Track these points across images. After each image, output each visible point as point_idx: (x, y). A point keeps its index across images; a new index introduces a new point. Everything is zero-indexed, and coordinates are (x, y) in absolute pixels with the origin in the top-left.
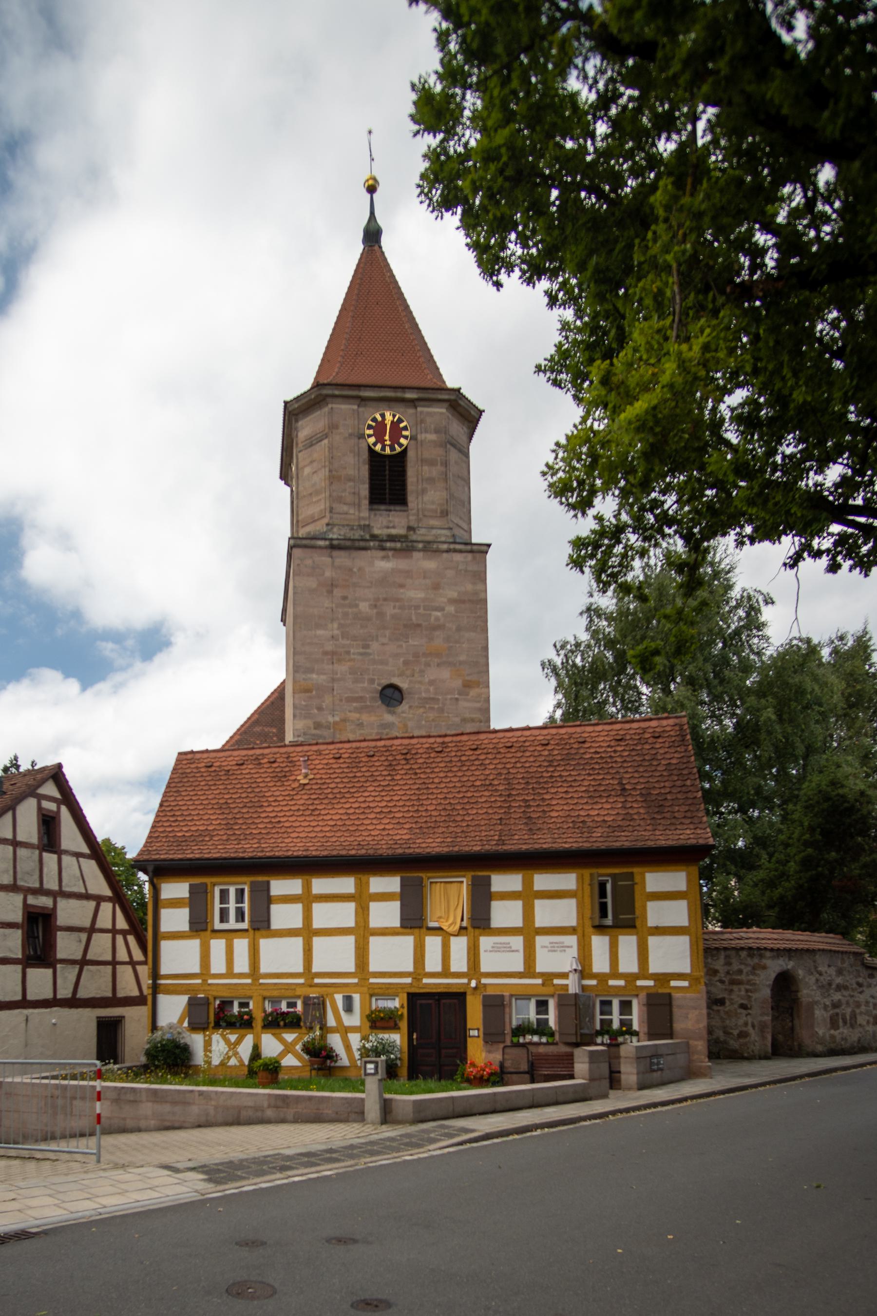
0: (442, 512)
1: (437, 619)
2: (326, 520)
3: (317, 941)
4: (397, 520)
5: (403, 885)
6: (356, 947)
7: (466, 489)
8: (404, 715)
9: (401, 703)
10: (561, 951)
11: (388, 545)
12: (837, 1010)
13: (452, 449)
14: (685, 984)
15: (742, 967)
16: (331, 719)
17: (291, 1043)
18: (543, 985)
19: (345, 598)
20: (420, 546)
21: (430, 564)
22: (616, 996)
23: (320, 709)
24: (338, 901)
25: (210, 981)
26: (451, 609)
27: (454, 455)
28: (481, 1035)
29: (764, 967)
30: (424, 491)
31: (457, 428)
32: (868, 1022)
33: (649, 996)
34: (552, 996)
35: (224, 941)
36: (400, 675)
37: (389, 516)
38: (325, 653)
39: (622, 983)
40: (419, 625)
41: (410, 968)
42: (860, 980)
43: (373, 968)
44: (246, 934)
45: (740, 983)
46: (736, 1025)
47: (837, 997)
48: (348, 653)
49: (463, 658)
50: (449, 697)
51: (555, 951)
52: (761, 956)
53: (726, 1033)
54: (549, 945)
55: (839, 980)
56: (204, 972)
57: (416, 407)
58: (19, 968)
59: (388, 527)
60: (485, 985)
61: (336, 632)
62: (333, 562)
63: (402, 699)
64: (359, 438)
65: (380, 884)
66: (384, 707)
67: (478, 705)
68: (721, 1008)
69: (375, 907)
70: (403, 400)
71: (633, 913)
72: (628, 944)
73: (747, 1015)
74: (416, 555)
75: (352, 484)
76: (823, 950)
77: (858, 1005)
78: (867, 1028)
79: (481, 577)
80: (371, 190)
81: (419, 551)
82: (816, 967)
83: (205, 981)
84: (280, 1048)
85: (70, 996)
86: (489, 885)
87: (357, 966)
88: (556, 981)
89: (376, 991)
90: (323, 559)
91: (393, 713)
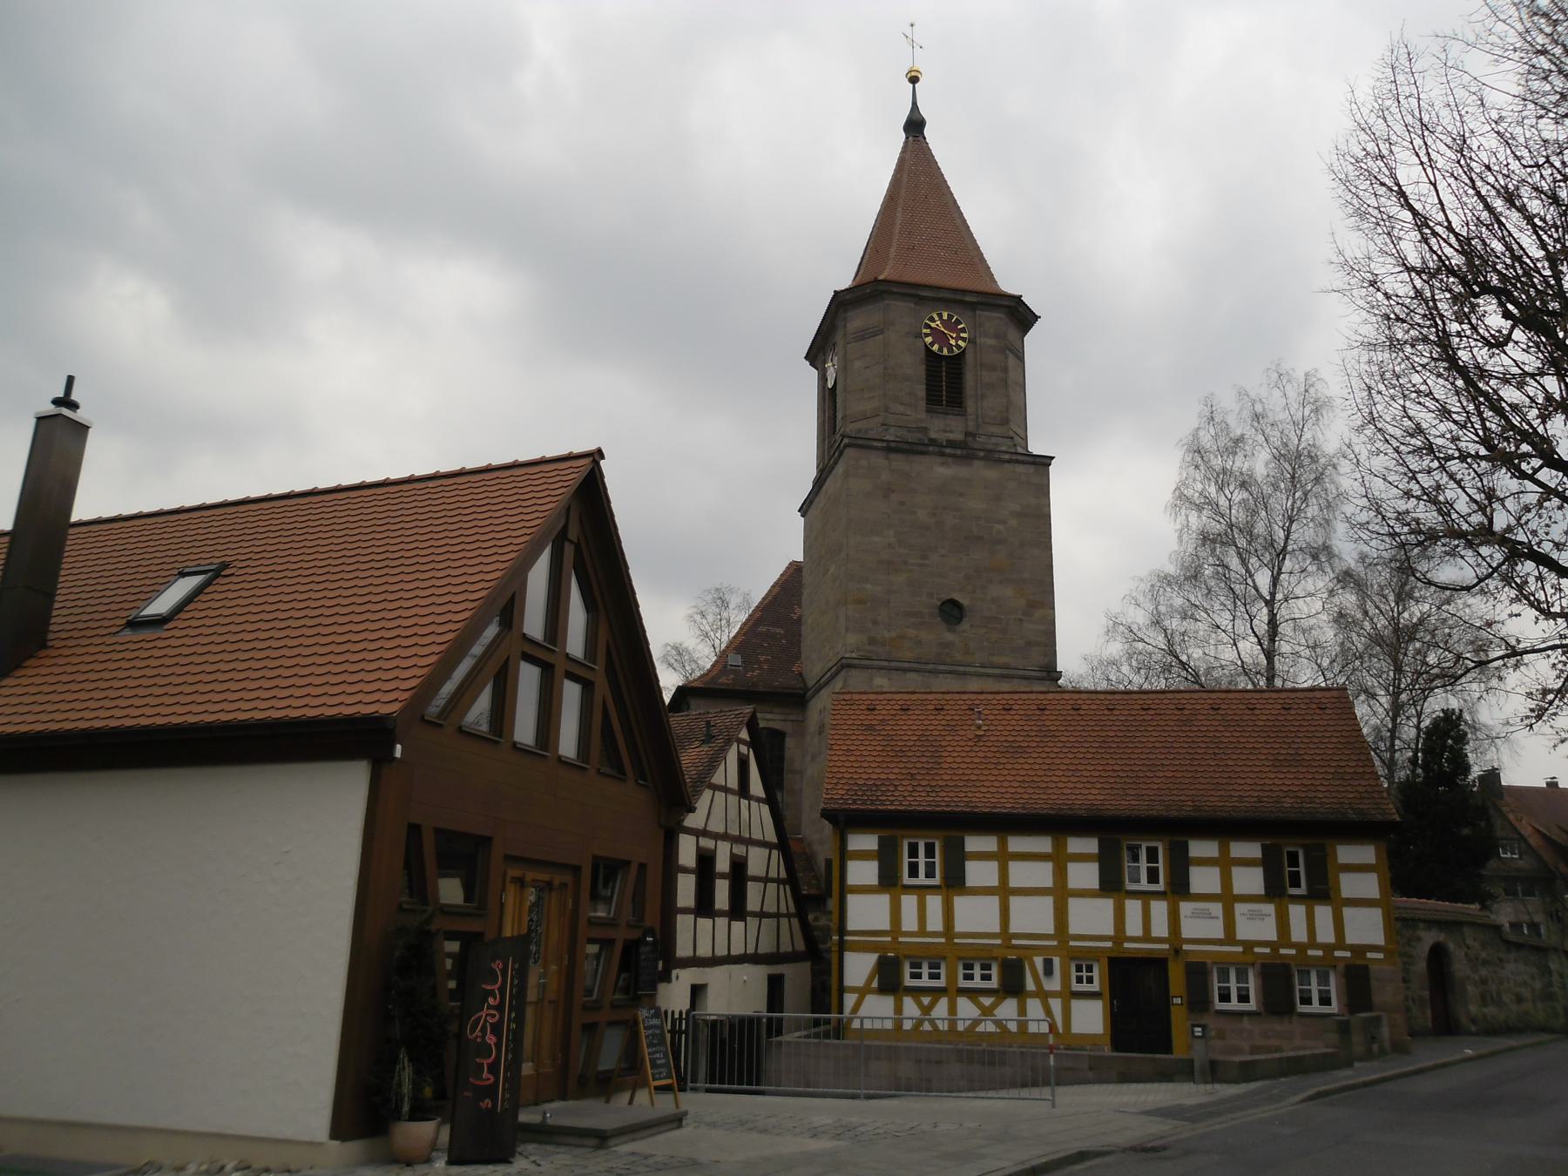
5: (1100, 847)
7: (1022, 394)
8: (965, 634)
10: (1260, 919)
11: (948, 451)
13: (1010, 354)
14: (1381, 956)
16: (887, 635)
19: (902, 503)
20: (982, 454)
21: (992, 474)
23: (875, 623)
25: (901, 939)
26: (1014, 522)
27: (1012, 360)
33: (1263, 965)
39: (1320, 953)
41: (1110, 931)
47: (1484, 972)
51: (1253, 919)
55: (1483, 955)
57: (974, 311)
58: (692, 917)
59: (945, 431)
60: (1187, 952)
64: (916, 337)
65: (1076, 845)
70: (961, 302)
71: (1327, 884)
72: (1323, 913)
74: (977, 463)
79: (1044, 491)
80: (914, 80)
82: (1464, 940)
83: (895, 939)
86: (1187, 851)
88: (1257, 950)
90: (878, 460)
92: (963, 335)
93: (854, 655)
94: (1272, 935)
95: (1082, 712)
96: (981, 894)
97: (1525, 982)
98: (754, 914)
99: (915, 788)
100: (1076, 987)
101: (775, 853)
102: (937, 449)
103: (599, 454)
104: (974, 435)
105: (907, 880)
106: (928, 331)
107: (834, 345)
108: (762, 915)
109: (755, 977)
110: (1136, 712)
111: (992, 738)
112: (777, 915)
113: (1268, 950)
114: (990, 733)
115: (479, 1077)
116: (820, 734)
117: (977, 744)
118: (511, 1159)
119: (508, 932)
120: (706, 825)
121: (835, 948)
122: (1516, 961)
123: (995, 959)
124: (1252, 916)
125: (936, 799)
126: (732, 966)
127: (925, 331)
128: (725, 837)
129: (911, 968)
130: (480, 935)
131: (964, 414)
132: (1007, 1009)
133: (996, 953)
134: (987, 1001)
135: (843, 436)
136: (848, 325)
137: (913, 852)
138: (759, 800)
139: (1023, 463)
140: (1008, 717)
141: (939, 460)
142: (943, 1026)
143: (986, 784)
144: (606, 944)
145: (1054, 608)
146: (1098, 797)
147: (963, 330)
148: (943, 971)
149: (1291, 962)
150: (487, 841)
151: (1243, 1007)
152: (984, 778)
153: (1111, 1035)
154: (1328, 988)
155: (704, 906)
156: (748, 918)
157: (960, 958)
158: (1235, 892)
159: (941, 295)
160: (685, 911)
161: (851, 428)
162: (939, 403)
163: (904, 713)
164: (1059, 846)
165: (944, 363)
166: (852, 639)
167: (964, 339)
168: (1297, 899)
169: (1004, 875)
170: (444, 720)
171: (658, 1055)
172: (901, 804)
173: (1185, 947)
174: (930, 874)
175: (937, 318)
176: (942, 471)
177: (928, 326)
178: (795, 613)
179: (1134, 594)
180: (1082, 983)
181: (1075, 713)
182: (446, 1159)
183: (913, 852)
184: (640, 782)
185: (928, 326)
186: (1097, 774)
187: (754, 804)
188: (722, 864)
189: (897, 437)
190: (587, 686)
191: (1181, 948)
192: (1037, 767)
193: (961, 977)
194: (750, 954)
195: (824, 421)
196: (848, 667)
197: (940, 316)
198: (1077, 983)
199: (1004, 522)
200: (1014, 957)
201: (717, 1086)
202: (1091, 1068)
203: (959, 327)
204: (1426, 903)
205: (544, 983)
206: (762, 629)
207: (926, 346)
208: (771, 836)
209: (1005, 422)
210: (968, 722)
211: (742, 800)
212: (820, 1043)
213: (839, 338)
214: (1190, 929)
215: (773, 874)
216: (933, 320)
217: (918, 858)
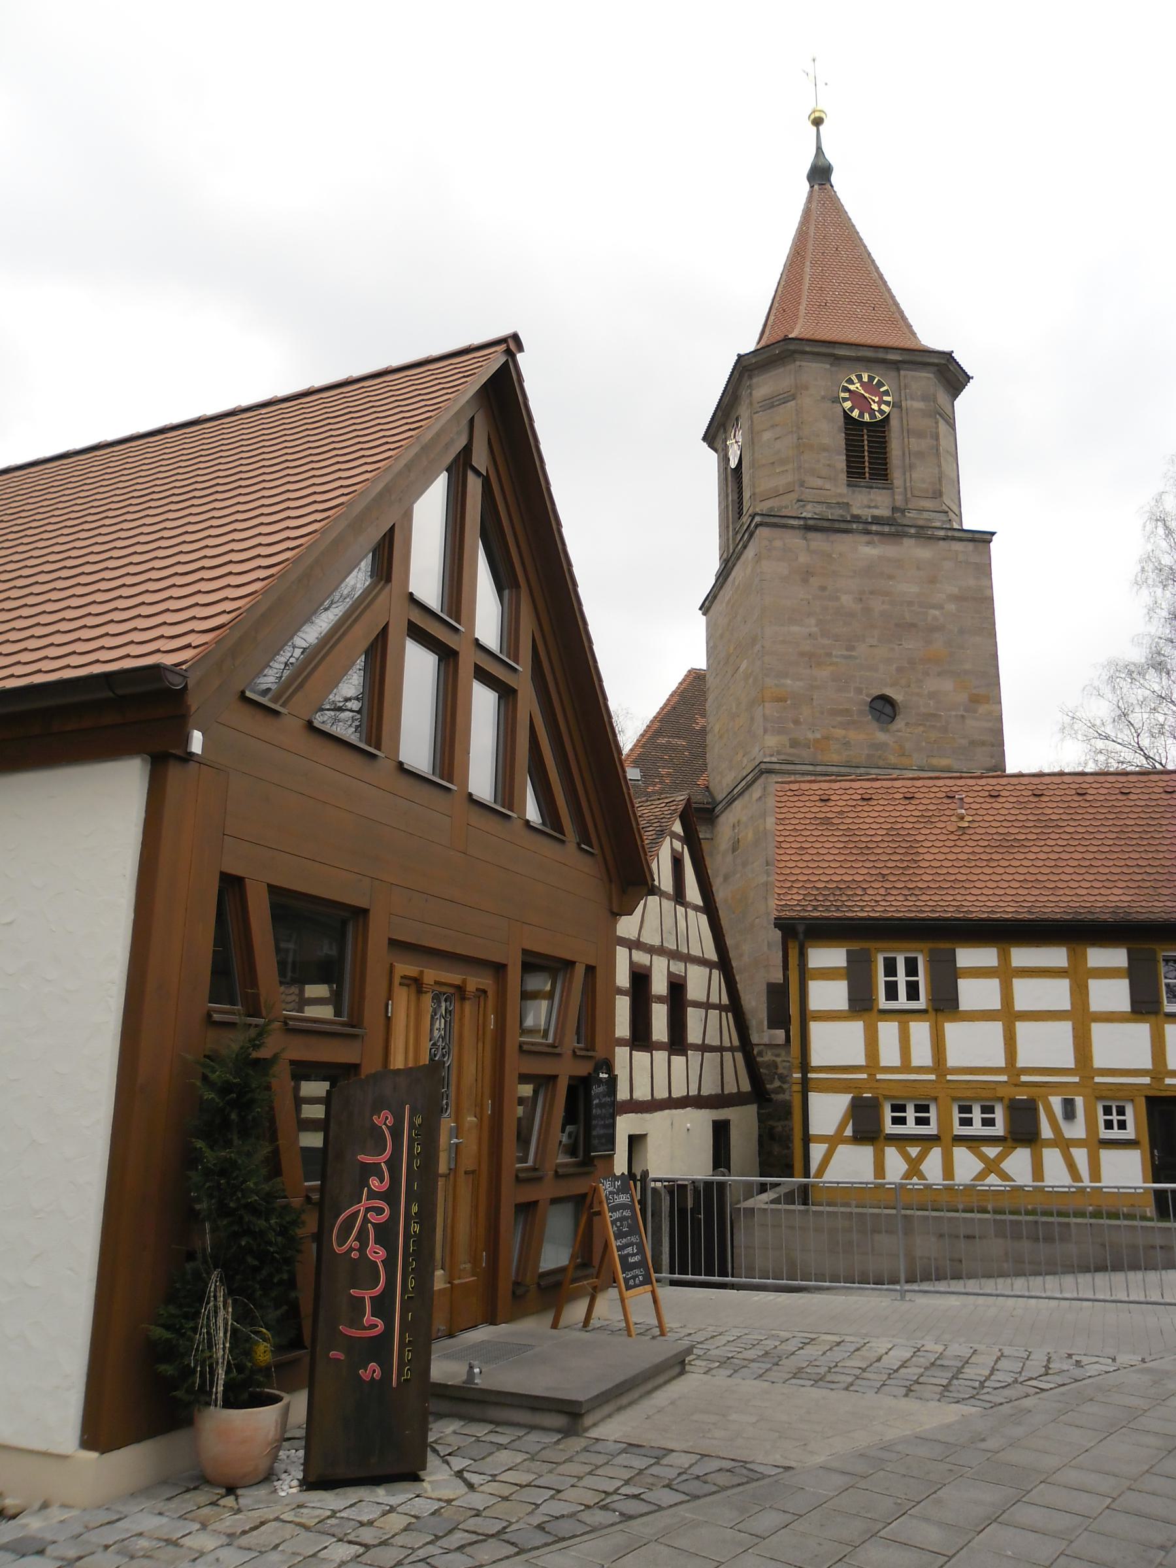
0: (934, 493)
1: (935, 618)
4: (879, 499)
5: (1130, 959)
6: (1074, 1037)
7: (955, 465)
8: (899, 734)
9: (893, 718)
11: (874, 528)
16: (810, 736)
17: (993, 1160)
19: (823, 588)
20: (913, 531)
23: (796, 722)
24: (1046, 977)
25: (879, 1077)
26: (951, 607)
27: (942, 426)
30: (911, 467)
36: (893, 685)
37: (869, 493)
38: (802, 654)
40: (913, 625)
44: (927, 1016)
48: (829, 655)
49: (968, 666)
50: (954, 713)
56: (870, 1065)
57: (898, 370)
59: (870, 507)
61: (814, 629)
62: (808, 546)
63: (895, 715)
64: (833, 402)
65: (1099, 957)
66: (875, 725)
67: (989, 725)
70: (884, 361)
74: (907, 542)
75: (825, 454)
79: (985, 570)
80: (818, 122)
81: (911, 536)
83: (872, 1076)
84: (1005, 1165)
85: (686, 1094)
89: (1104, 1093)
90: (794, 540)
91: (887, 731)
92: (885, 398)
93: (774, 759)
95: (1089, 798)
96: (978, 1019)
98: (696, 1047)
99: (889, 891)
100: (1105, 1134)
101: (715, 973)
102: (861, 526)
103: (512, 344)
104: (903, 511)
105: (883, 1003)
107: (737, 419)
108: (704, 1048)
109: (699, 1122)
110: (1158, 796)
111: (979, 831)
112: (720, 1049)
114: (976, 825)
115: (356, 1322)
116: (733, 852)
117: (961, 837)
118: (421, 1473)
119: (398, 1061)
120: (639, 935)
121: (797, 1088)
123: (1001, 1099)
125: (918, 903)
126: (674, 1111)
127: (843, 395)
128: (660, 951)
129: (960, 1112)
130: (354, 1068)
131: (890, 487)
132: (1018, 1163)
134: (992, 1152)
135: (753, 516)
136: (754, 392)
137: (891, 969)
138: (696, 908)
139: (961, 540)
140: (996, 805)
141: (866, 538)
143: (978, 884)
144: (544, 1082)
145: (999, 702)
146: (1123, 898)
147: (886, 393)
148: (933, 1114)
150: (363, 913)
152: (975, 878)
155: (640, 1038)
156: (689, 1052)
157: (955, 1099)
159: (860, 354)
160: (621, 1042)
161: (763, 507)
162: (861, 475)
163: (865, 803)
164: (1077, 960)
165: (865, 431)
166: (771, 741)
167: (887, 403)
169: (1007, 995)
170: (282, 705)
171: (629, 1250)
174: (913, 993)
175: (856, 380)
176: (867, 551)
177: (846, 390)
178: (697, 723)
179: (1096, 683)
180: (1112, 1128)
181: (1080, 798)
182: (300, 1476)
183: (891, 969)
184: (583, 846)
185: (846, 390)
186: (1119, 870)
187: (691, 912)
188: (659, 986)
189: (815, 513)
190: (506, 694)
192: (1040, 863)
193: (956, 1122)
194: (694, 1096)
195: (727, 506)
196: (767, 772)
197: (860, 378)
198: (1106, 1128)
199: (940, 607)
200: (1025, 1097)
201: (703, 1278)
203: (882, 390)
205: (457, 1145)
206: (662, 740)
207: (844, 410)
208: (712, 955)
209: (938, 494)
210: (947, 812)
211: (677, 906)
212: (807, 1211)
213: (743, 411)
215: (714, 999)
216: (850, 381)
217: (896, 976)
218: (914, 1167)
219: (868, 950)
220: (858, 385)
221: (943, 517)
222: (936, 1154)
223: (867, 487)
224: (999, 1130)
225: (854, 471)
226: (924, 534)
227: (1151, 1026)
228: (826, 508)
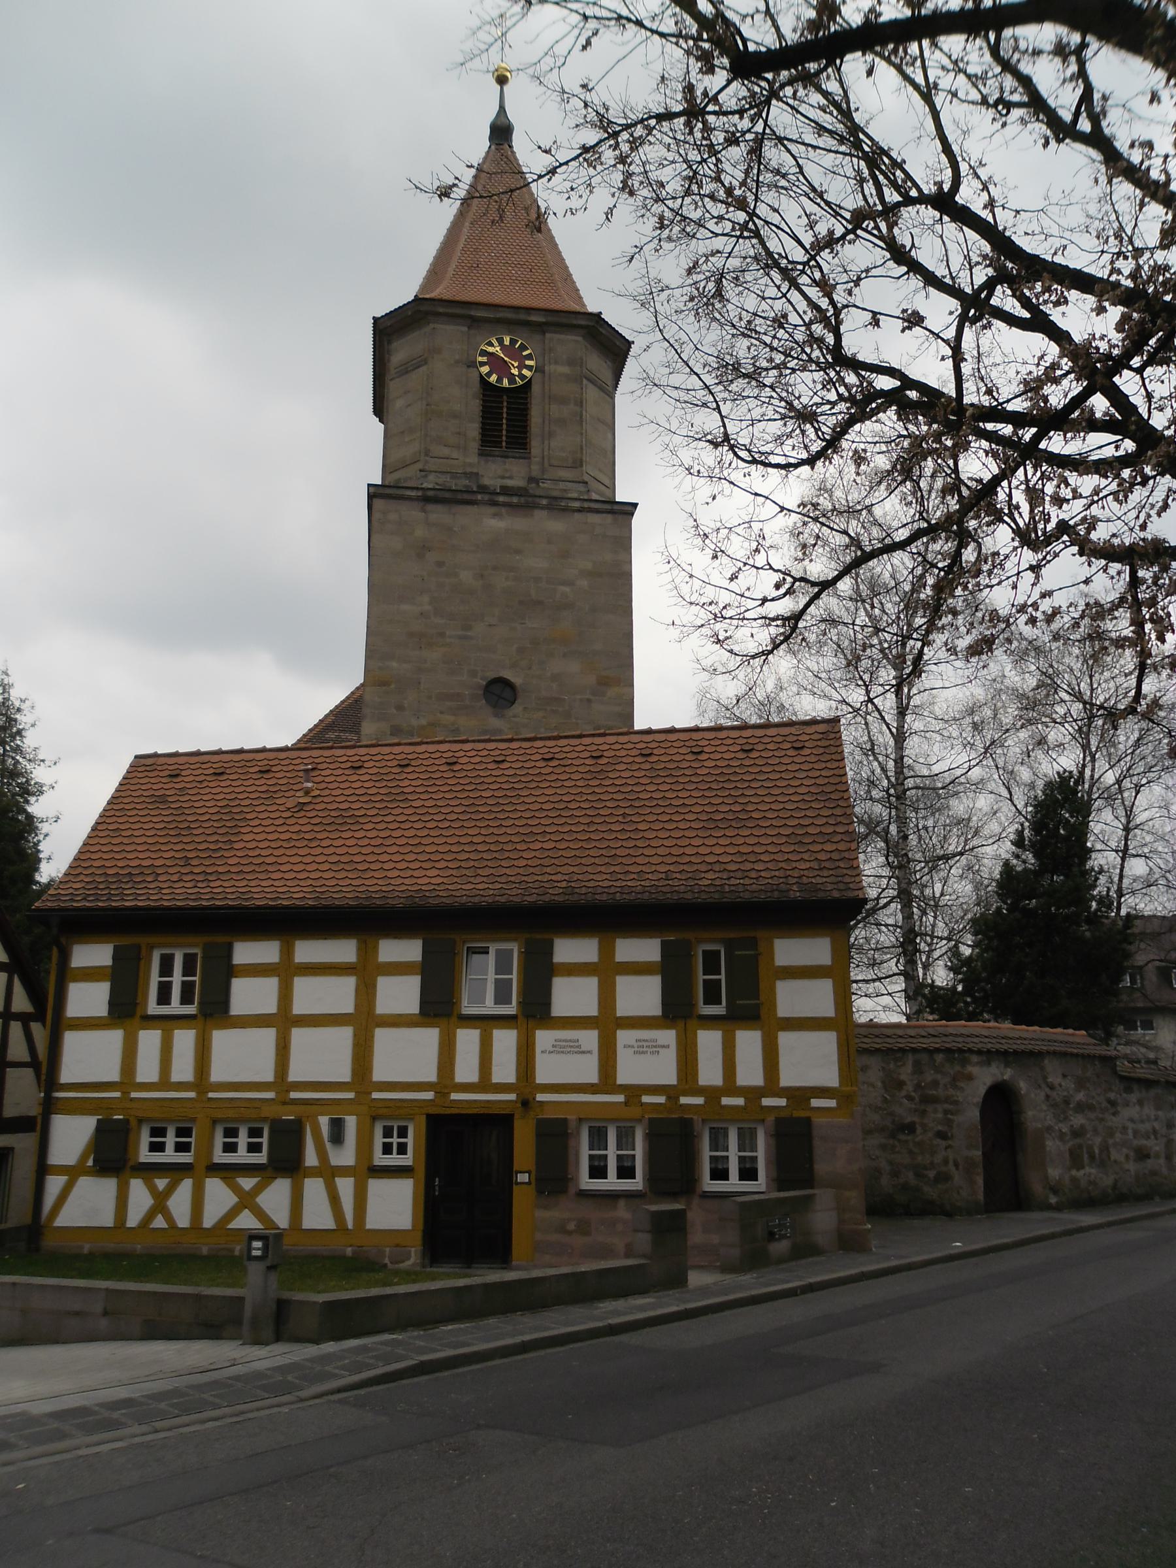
2: (419, 466)
3: (299, 1036)
9: (513, 703)
10: (652, 1053)
11: (501, 499)
12: (1078, 1141)
13: (590, 386)
14: (832, 1103)
15: (939, 1077)
16: (414, 722)
17: (248, 1193)
18: (626, 1103)
19: (440, 564)
20: (544, 502)
21: (556, 525)
22: (733, 1121)
23: (400, 708)
24: (331, 974)
25: (134, 1095)
26: (584, 583)
27: (591, 393)
28: (533, 1181)
29: (970, 1078)
30: (551, 435)
31: (597, 363)
32: (1127, 1157)
33: (779, 1121)
34: (639, 1121)
35: (159, 1032)
37: (505, 463)
39: (740, 1101)
40: (540, 603)
41: (431, 1076)
42: (1112, 1096)
43: (378, 1075)
44: (194, 1022)
45: (935, 1100)
46: (932, 1163)
47: (1078, 1120)
48: (442, 635)
50: (578, 697)
51: (643, 1053)
52: (964, 1062)
53: (918, 1175)
54: (636, 1045)
55: (1080, 1096)
57: (544, 333)
59: (503, 477)
64: (469, 367)
68: (910, 1138)
69: (623, 984)
72: (749, 1042)
73: (946, 1148)
74: (539, 514)
76: (1055, 1053)
77: (1111, 1134)
78: (1126, 1166)
79: (624, 544)
80: (502, 80)
81: (543, 508)
82: (1045, 1078)
83: (125, 1093)
87: (355, 1072)
88: (646, 1099)
89: (384, 1111)
92: (528, 363)
94: (669, 1076)
97: (1155, 1132)
100: (380, 1159)
102: (486, 497)
105: (153, 1008)
106: (485, 359)
113: (661, 1099)
122: (1140, 1103)
124: (641, 1049)
127: (480, 359)
131: (528, 457)
133: (267, 1112)
134: (247, 1183)
137: (166, 967)
141: (493, 510)
142: (183, 1220)
145: (632, 685)
149: (695, 1117)
151: (626, 1185)
153: (424, 1231)
154: (620, 1152)
158: (620, 1013)
159: (499, 315)
162: (498, 444)
164: (367, 953)
165: (505, 397)
167: (529, 368)
168: (710, 1021)
172: (149, 899)
173: (540, 1097)
175: (496, 344)
176: (494, 523)
177: (484, 353)
183: (166, 967)
189: (437, 484)
191: (534, 1099)
197: (500, 341)
198: (384, 1154)
199: (570, 583)
202: (106, 1313)
204: (947, 1026)
214: (548, 1070)
218: (160, 1205)
219: (139, 947)
220: (498, 349)
221: (581, 488)
222: (186, 1187)
223: (502, 457)
224: (261, 1158)
225: (490, 441)
226: (557, 505)
227: (441, 1032)
228: (451, 478)
